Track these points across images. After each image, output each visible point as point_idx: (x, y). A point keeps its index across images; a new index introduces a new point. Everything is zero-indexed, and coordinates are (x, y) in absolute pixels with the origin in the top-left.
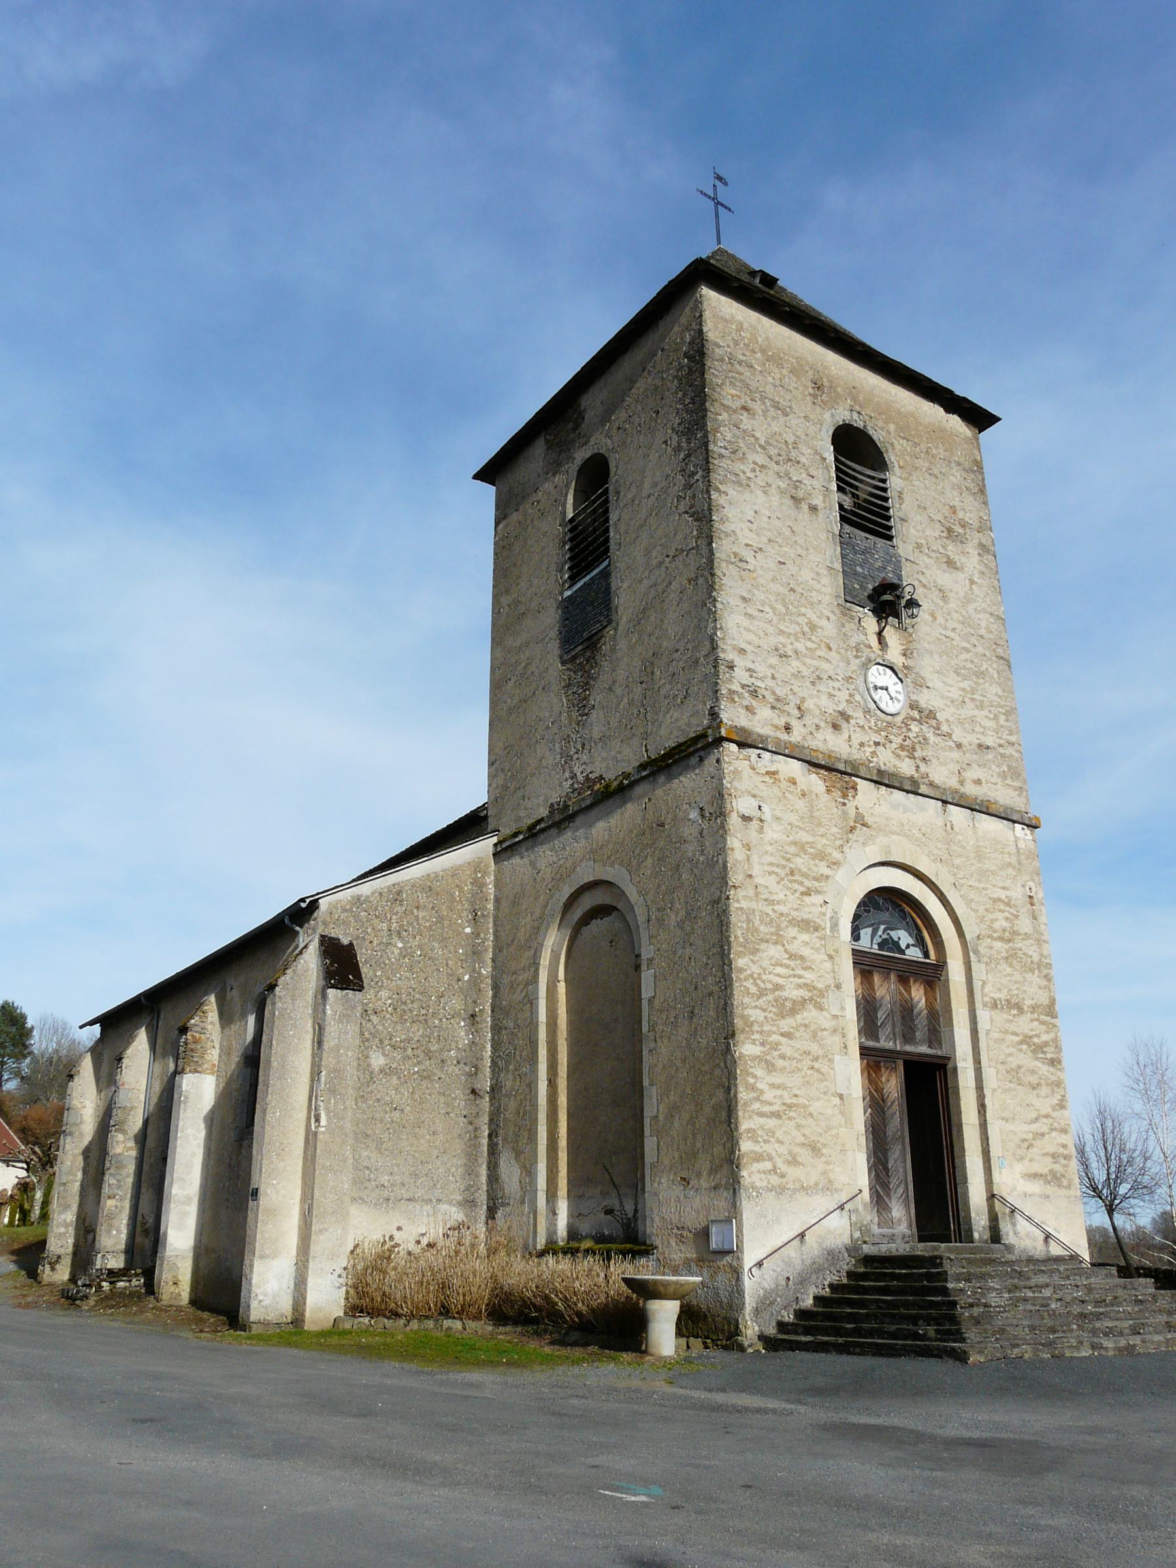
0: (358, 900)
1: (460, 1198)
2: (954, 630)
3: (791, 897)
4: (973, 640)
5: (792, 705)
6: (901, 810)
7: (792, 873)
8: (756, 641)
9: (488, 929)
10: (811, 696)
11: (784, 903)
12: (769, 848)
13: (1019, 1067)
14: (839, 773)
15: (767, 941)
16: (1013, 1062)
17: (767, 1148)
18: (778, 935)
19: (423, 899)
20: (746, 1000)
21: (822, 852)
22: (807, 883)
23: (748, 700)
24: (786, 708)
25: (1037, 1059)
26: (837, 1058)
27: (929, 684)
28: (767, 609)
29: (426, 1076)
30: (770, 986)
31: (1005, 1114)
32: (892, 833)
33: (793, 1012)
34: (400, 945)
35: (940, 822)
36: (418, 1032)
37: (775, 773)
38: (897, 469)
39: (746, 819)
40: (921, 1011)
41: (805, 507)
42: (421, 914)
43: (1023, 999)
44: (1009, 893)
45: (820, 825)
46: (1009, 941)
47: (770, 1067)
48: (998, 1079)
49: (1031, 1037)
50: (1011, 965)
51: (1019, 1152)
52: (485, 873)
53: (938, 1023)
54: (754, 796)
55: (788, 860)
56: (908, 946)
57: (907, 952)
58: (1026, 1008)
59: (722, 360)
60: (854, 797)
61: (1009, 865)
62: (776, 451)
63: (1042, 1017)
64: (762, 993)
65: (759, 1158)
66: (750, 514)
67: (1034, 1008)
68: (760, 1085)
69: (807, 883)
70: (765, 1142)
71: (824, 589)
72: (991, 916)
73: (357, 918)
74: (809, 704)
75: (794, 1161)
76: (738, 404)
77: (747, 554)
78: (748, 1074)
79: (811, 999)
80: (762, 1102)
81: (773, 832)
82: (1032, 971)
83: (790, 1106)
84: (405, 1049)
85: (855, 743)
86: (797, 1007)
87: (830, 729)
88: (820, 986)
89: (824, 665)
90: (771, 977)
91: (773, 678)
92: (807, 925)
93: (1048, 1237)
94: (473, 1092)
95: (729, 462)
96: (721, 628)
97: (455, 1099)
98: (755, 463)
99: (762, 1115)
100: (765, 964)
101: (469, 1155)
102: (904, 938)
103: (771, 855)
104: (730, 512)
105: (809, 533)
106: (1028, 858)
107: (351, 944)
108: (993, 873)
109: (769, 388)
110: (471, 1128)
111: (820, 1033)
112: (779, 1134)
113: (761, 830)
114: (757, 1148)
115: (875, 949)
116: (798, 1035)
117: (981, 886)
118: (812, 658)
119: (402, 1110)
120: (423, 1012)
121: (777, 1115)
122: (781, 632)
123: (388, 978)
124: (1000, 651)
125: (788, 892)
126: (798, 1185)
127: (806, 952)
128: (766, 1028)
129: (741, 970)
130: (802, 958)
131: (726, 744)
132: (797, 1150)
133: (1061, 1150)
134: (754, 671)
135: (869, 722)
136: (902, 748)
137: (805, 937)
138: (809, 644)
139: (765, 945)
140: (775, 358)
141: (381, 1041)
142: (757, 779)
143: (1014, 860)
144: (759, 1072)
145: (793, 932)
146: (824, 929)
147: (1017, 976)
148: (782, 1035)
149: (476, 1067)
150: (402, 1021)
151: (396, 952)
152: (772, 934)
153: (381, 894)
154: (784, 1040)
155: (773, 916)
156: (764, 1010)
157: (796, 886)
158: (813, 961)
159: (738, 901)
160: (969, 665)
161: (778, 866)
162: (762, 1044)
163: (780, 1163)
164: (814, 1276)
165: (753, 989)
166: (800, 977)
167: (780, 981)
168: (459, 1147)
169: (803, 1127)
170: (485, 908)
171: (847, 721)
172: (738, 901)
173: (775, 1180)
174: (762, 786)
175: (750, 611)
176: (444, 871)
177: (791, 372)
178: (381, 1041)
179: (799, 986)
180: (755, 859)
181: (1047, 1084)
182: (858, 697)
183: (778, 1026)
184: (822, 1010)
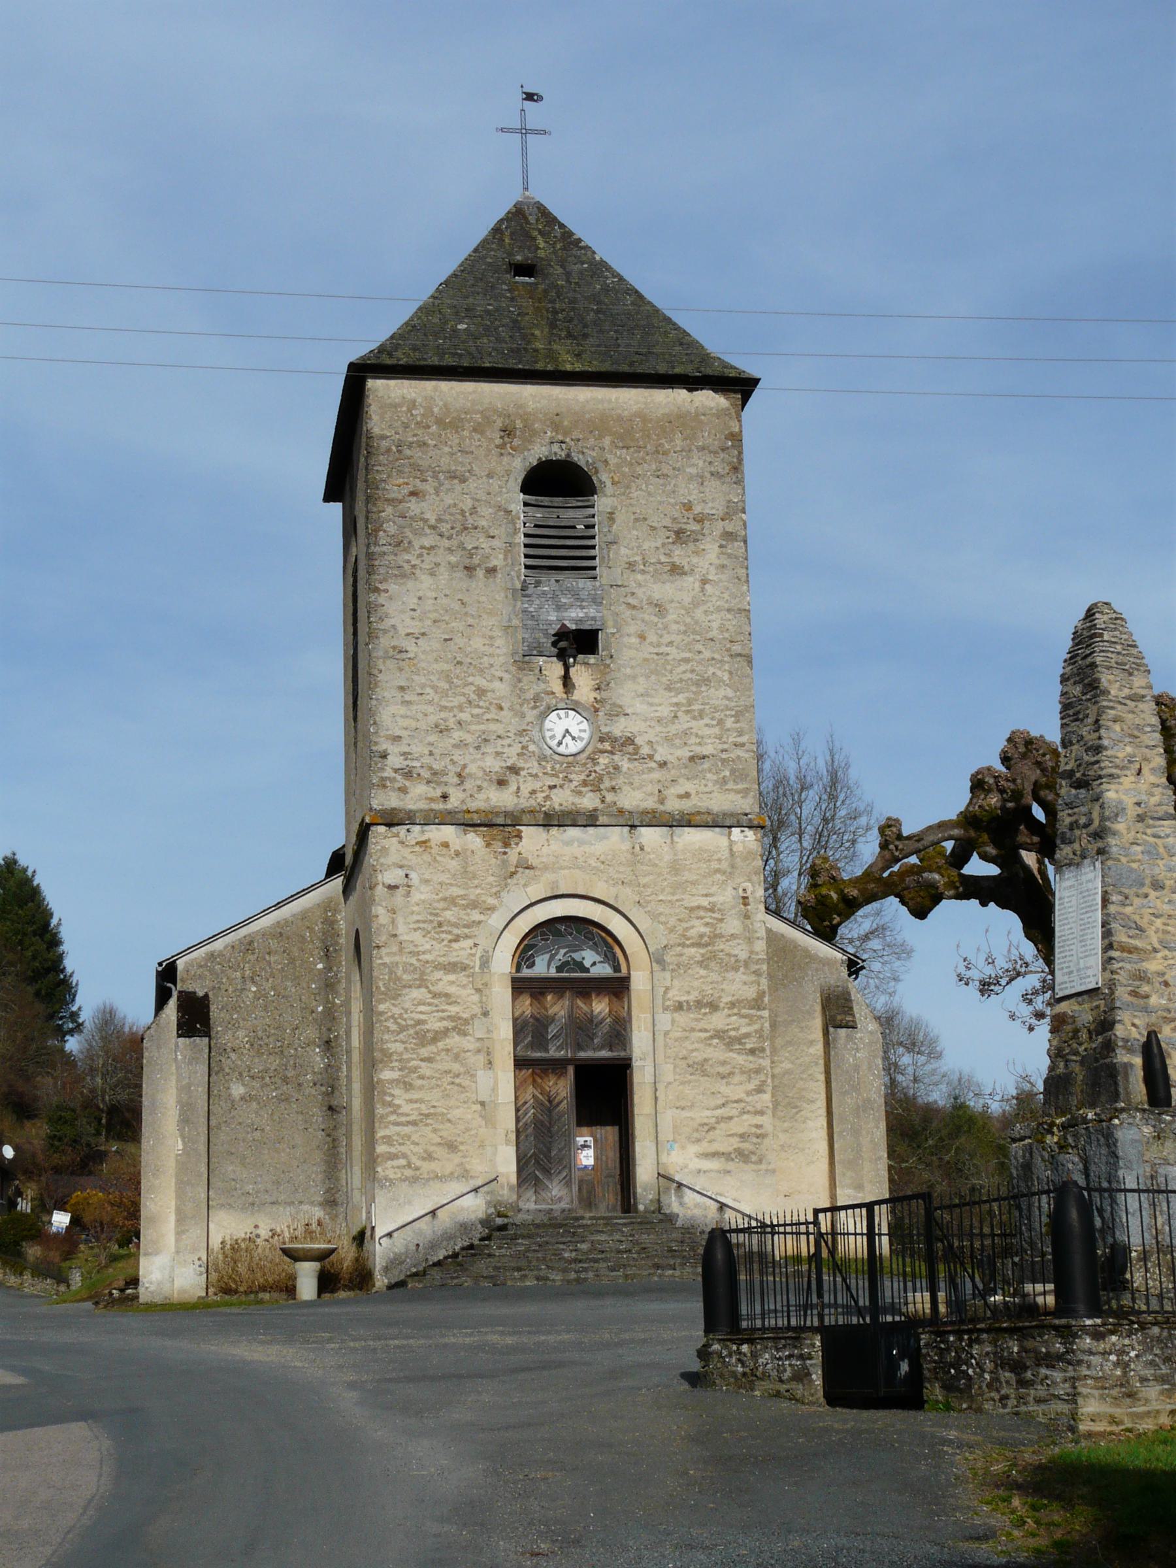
0: (212, 956)
1: (321, 1199)
2: (671, 643)
3: (437, 946)
4: (699, 647)
5: (451, 774)
6: (576, 844)
7: (440, 925)
8: (414, 724)
9: (340, 962)
10: (474, 761)
11: (430, 952)
12: (416, 908)
13: (706, 1060)
14: (500, 826)
15: (410, 987)
16: (698, 1056)
17: (403, 1149)
18: (422, 980)
19: (274, 944)
20: (386, 1037)
21: (474, 901)
22: (456, 931)
23: (400, 781)
24: (445, 779)
25: (732, 1050)
26: (480, 1073)
27: (629, 711)
28: (428, 690)
29: (284, 1099)
30: (410, 1022)
31: (682, 1103)
32: (562, 868)
33: (435, 1040)
34: (254, 989)
35: (626, 846)
36: (274, 1062)
37: (424, 842)
38: (609, 489)
39: (392, 888)
40: (603, 1020)
41: (480, 573)
42: (273, 959)
43: (720, 997)
44: (711, 899)
45: (474, 877)
46: (707, 945)
47: (408, 1087)
48: (675, 1073)
49: (724, 1032)
50: (706, 968)
51: (696, 1135)
52: (336, 911)
53: (620, 1032)
54: (401, 867)
55: (436, 915)
56: (594, 964)
57: (593, 970)
58: (722, 1005)
59: (389, 450)
60: (517, 844)
61: (718, 871)
62: (449, 526)
63: (743, 1011)
64: (403, 1029)
65: (393, 1157)
66: (412, 602)
67: (732, 1005)
68: (397, 1102)
69: (456, 931)
70: (400, 1144)
71: (498, 651)
72: (685, 925)
73: (212, 971)
74: (472, 768)
75: (429, 1157)
76: (405, 490)
77: (409, 645)
78: (385, 1094)
79: (454, 1029)
80: (398, 1114)
81: (421, 894)
82: (736, 969)
83: (427, 1116)
84: (263, 1078)
85: (525, 791)
86: (438, 1036)
87: (494, 787)
88: (465, 1016)
89: (492, 727)
90: (413, 1015)
91: (431, 754)
92: (452, 968)
93: (722, 1207)
94: (331, 1108)
95: (392, 557)
96: (375, 723)
97: (313, 1116)
98: (422, 547)
99: (397, 1124)
100: (407, 1005)
101: (327, 1162)
102: (588, 957)
103: (419, 914)
104: (391, 608)
105: (483, 599)
106: (745, 859)
107: (206, 996)
108: (693, 883)
109: (445, 461)
110: (328, 1139)
111: (463, 1054)
112: (415, 1138)
113: (408, 894)
114: (393, 1150)
115: (553, 972)
116: (438, 1058)
117: (675, 898)
118: (479, 723)
119: (263, 1130)
120: (279, 1044)
121: (414, 1123)
122: (443, 708)
123: (244, 1019)
124: (737, 648)
125: (434, 943)
126: (432, 1175)
127: (452, 990)
128: (405, 1057)
129: (382, 1013)
130: (447, 995)
131: (373, 828)
132: (432, 1149)
133: (754, 1130)
134: (409, 753)
135: (545, 768)
136: (585, 783)
137: (452, 977)
138: (476, 711)
139: (407, 990)
140: (451, 422)
141: (241, 1074)
142: (406, 852)
143: (725, 865)
144: (396, 1092)
145: (439, 974)
146: (473, 967)
147: (714, 976)
148: (422, 1060)
149: (333, 1087)
150: (259, 1054)
151: (251, 995)
152: (415, 980)
153: (233, 947)
154: (423, 1064)
155: (417, 964)
156: (403, 1042)
157: (443, 936)
158: (459, 997)
159: (381, 958)
160: (689, 675)
161: (424, 922)
162: (400, 1070)
163: (414, 1159)
164: (445, 1243)
165: (394, 1027)
166: (443, 1011)
167: (422, 1017)
168: (318, 1156)
169: (439, 1130)
170: (337, 943)
171: (517, 773)
172: (381, 958)
173: (408, 1173)
174: (410, 856)
175: (407, 698)
176: (294, 916)
177: (475, 430)
178: (241, 1074)
179: (442, 1019)
180: (400, 920)
181: (743, 1072)
182: (532, 748)
183: (418, 1054)
184: (465, 1035)
